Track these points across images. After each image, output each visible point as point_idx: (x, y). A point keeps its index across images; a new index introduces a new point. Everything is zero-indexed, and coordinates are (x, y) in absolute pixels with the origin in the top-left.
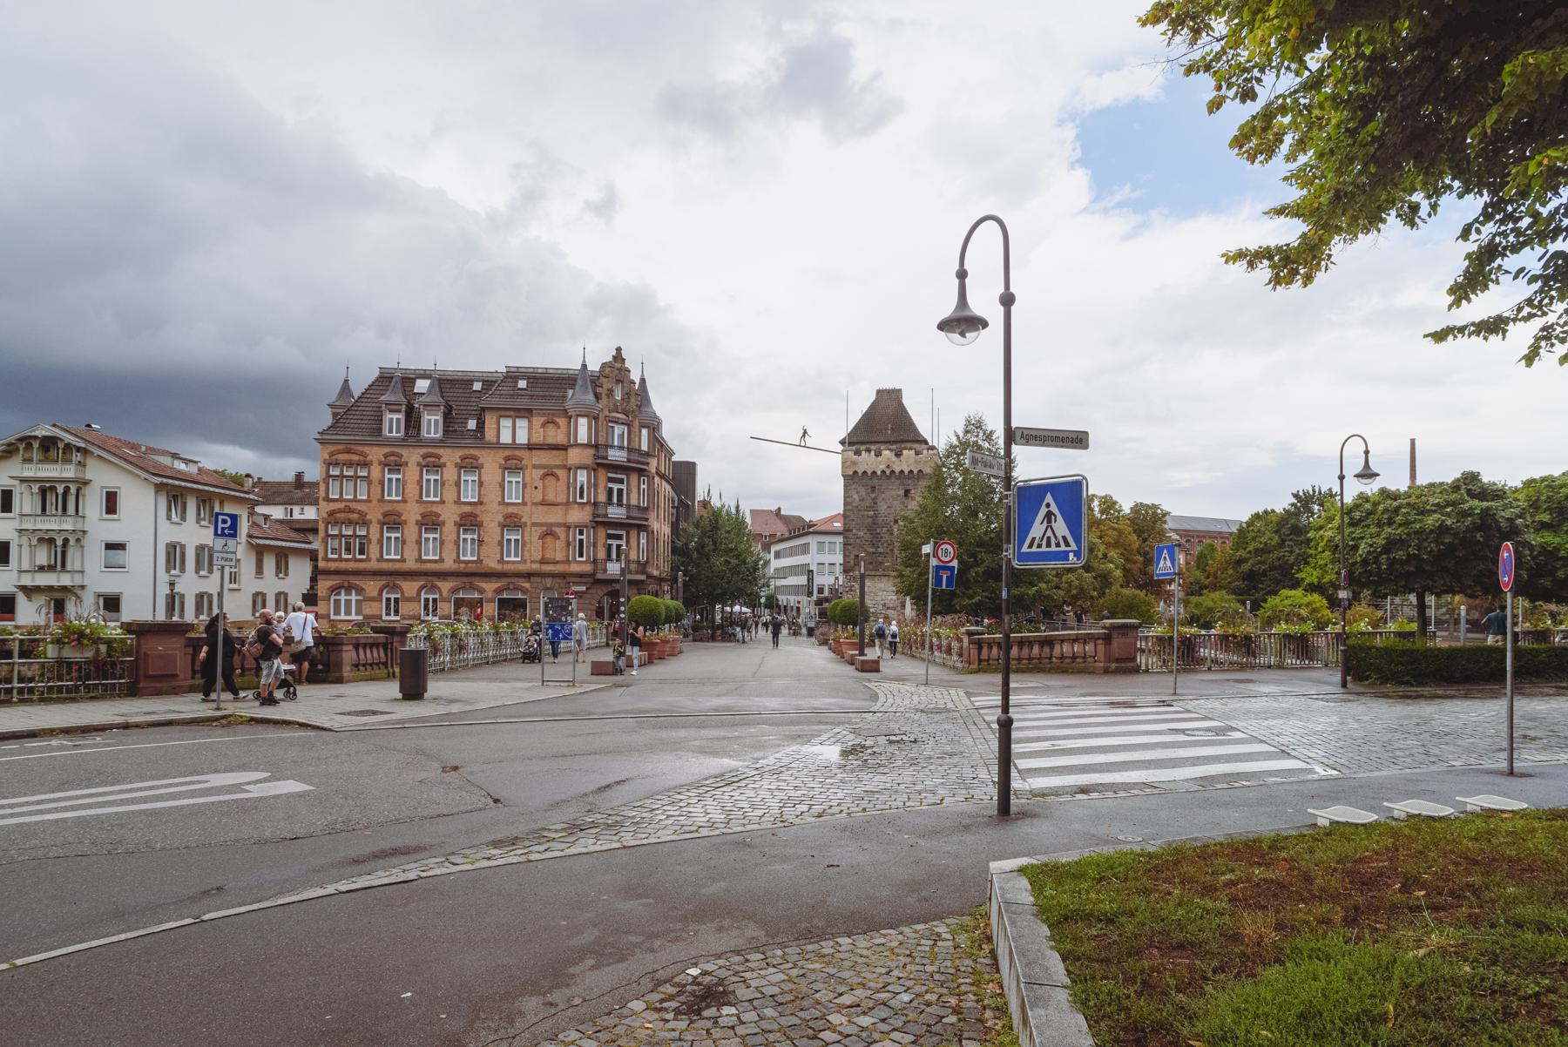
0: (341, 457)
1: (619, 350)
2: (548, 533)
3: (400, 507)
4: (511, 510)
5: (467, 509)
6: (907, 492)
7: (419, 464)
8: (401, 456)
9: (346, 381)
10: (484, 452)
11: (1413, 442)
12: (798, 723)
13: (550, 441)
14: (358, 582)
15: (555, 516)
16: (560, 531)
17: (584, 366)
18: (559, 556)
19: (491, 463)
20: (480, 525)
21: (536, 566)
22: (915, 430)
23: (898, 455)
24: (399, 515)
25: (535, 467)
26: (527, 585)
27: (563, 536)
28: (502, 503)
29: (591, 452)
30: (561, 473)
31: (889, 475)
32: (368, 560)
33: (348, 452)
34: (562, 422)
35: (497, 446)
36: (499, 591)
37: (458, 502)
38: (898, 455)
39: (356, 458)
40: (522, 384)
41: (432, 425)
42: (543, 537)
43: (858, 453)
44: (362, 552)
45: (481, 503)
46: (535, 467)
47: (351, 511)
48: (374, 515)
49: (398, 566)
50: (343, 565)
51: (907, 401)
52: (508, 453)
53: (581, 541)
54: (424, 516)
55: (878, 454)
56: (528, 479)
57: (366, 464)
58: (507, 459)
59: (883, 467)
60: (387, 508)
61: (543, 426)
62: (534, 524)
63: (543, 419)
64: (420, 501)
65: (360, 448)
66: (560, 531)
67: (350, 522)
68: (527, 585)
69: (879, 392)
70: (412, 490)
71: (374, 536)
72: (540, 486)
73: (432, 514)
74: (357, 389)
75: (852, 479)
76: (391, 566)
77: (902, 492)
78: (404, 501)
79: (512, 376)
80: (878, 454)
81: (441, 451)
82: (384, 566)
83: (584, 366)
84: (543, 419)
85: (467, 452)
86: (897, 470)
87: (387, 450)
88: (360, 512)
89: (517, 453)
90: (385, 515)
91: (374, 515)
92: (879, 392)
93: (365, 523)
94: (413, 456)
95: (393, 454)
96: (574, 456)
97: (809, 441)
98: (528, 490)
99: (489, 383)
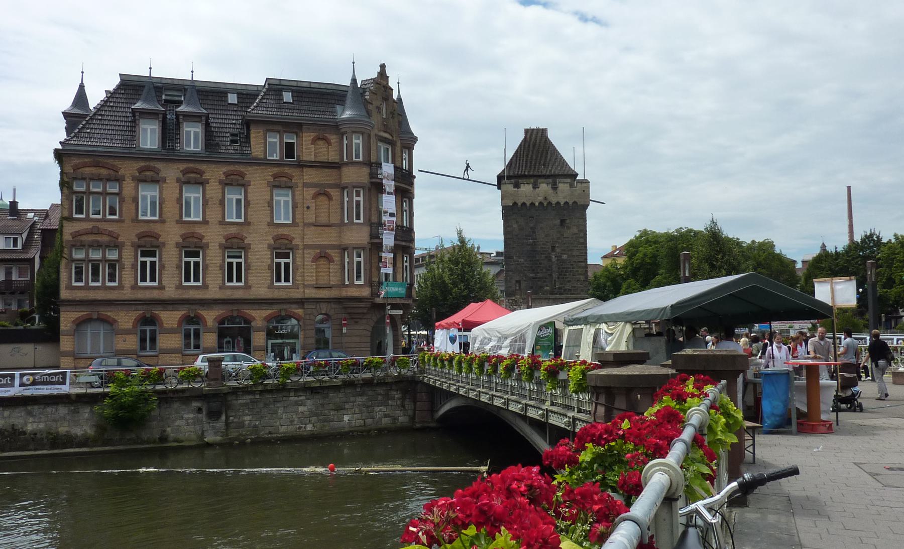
0: (87, 170)
1: (383, 66)
2: (323, 256)
3: (157, 228)
4: (281, 231)
5: (233, 230)
6: (563, 222)
7: (178, 180)
8: (157, 171)
9: (82, 87)
10: (250, 169)
11: (849, 188)
12: (51, 383)
13: (322, 158)
14: (110, 313)
15: (329, 238)
16: (334, 254)
17: (354, 81)
18: (334, 280)
19: (258, 179)
20: (246, 248)
21: (311, 293)
22: (563, 163)
23: (555, 187)
24: (157, 236)
25: (305, 185)
26: (300, 312)
27: (337, 258)
28: (271, 224)
29: (366, 170)
30: (334, 193)
31: (546, 206)
32: (121, 287)
33: (97, 165)
34: (333, 139)
35: (263, 163)
36: (268, 319)
37: (222, 223)
38: (555, 187)
39: (104, 172)
40: (287, 97)
41: (192, 137)
42: (316, 259)
43: (517, 186)
44: (112, 278)
45: (247, 223)
46: (305, 185)
47: (99, 232)
48: (128, 235)
49: (155, 295)
50: (92, 295)
51: (551, 136)
52: (276, 170)
53: (359, 263)
54: (185, 237)
55: (535, 186)
56: (298, 198)
57: (119, 180)
58: (275, 176)
59: (541, 198)
60: (143, 229)
61: (314, 142)
62: (306, 247)
63: (313, 135)
64: (180, 222)
65: (111, 161)
66: (334, 254)
67: (96, 246)
68: (300, 312)
69: (526, 131)
70: (171, 209)
71: (128, 260)
72: (313, 207)
73: (192, 235)
74: (95, 98)
75: (510, 212)
76: (148, 295)
77: (558, 222)
78: (162, 221)
79: (275, 88)
80: (535, 186)
81: (203, 167)
82: (140, 295)
83: (354, 81)
84: (313, 135)
85: (231, 168)
86: (554, 201)
87: (142, 164)
88: (110, 234)
89: (286, 170)
90: (141, 236)
91: (128, 235)
92: (526, 131)
93: (116, 245)
94: (171, 172)
95: (148, 169)
96: (351, 175)
97: (472, 175)
98: (299, 211)
99: (247, 94)
